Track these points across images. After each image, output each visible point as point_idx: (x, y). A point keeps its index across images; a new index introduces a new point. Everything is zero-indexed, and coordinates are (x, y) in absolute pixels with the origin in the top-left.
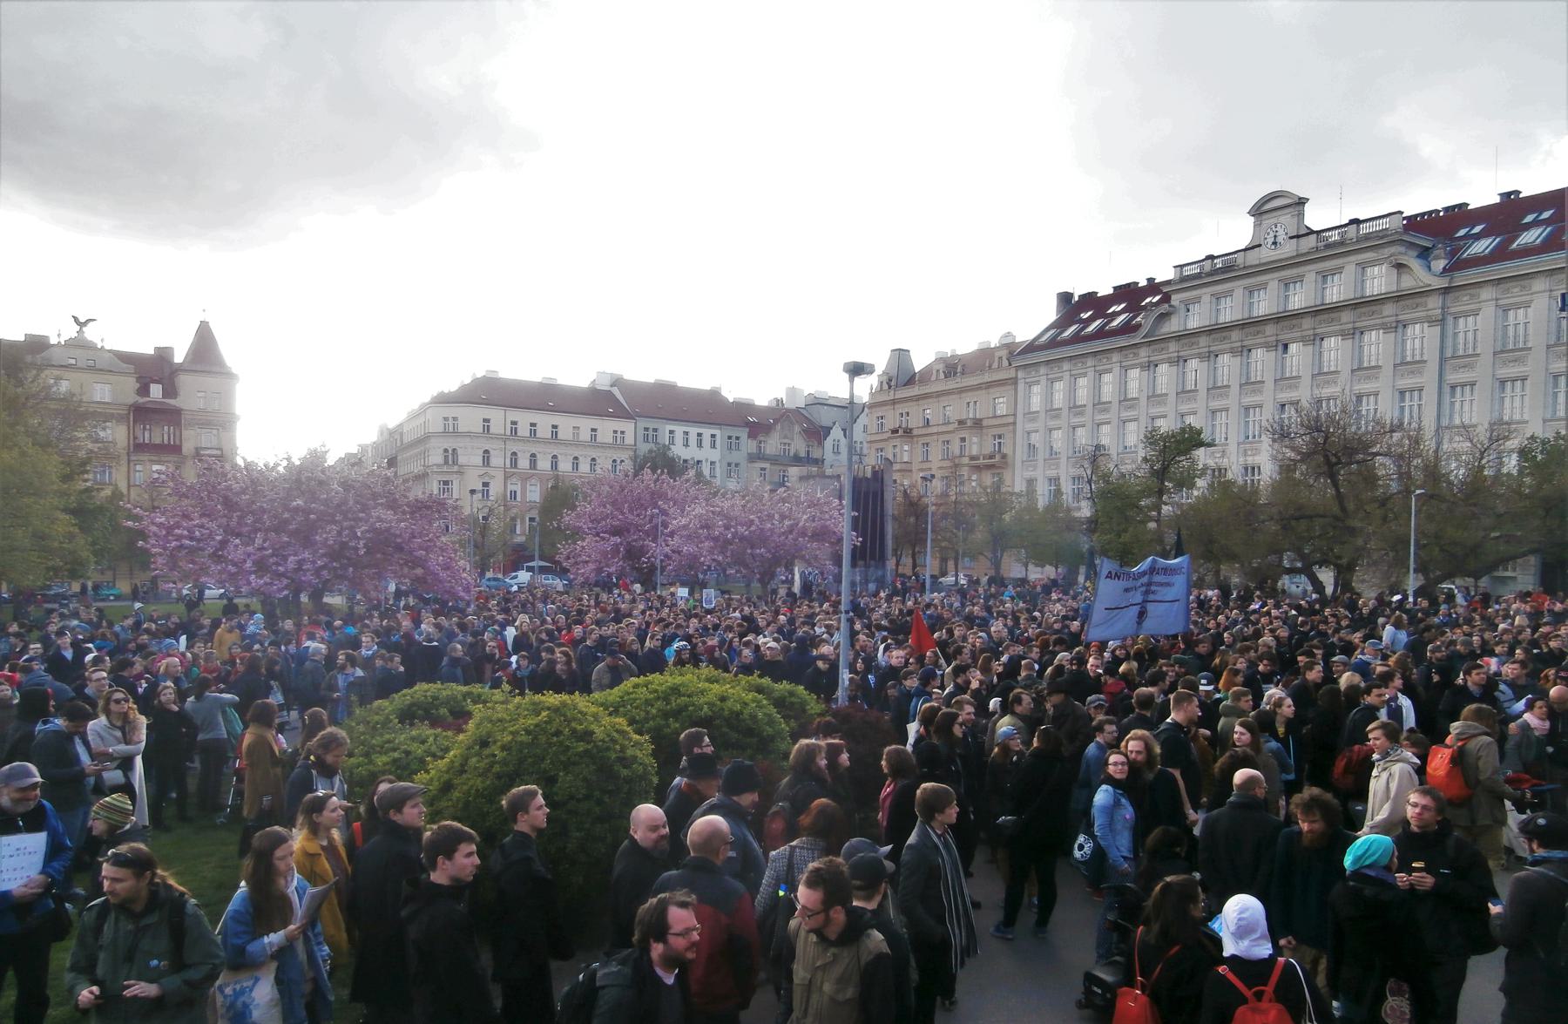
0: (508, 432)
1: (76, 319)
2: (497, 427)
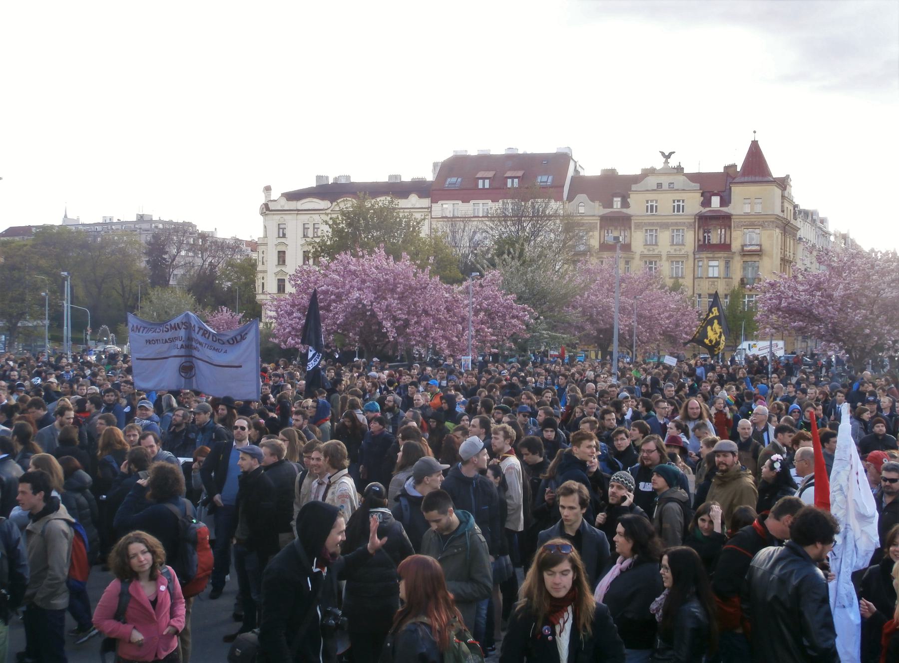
1: (663, 154)
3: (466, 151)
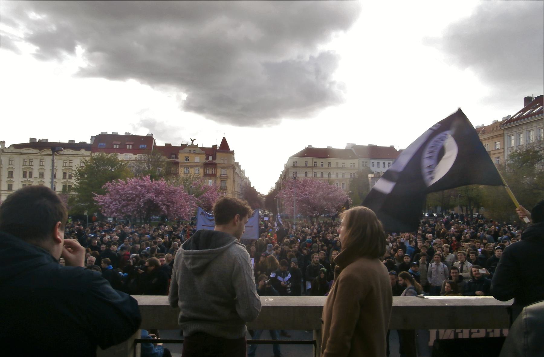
0: (314, 166)
1: (191, 139)
2: (310, 164)
3: (117, 133)
